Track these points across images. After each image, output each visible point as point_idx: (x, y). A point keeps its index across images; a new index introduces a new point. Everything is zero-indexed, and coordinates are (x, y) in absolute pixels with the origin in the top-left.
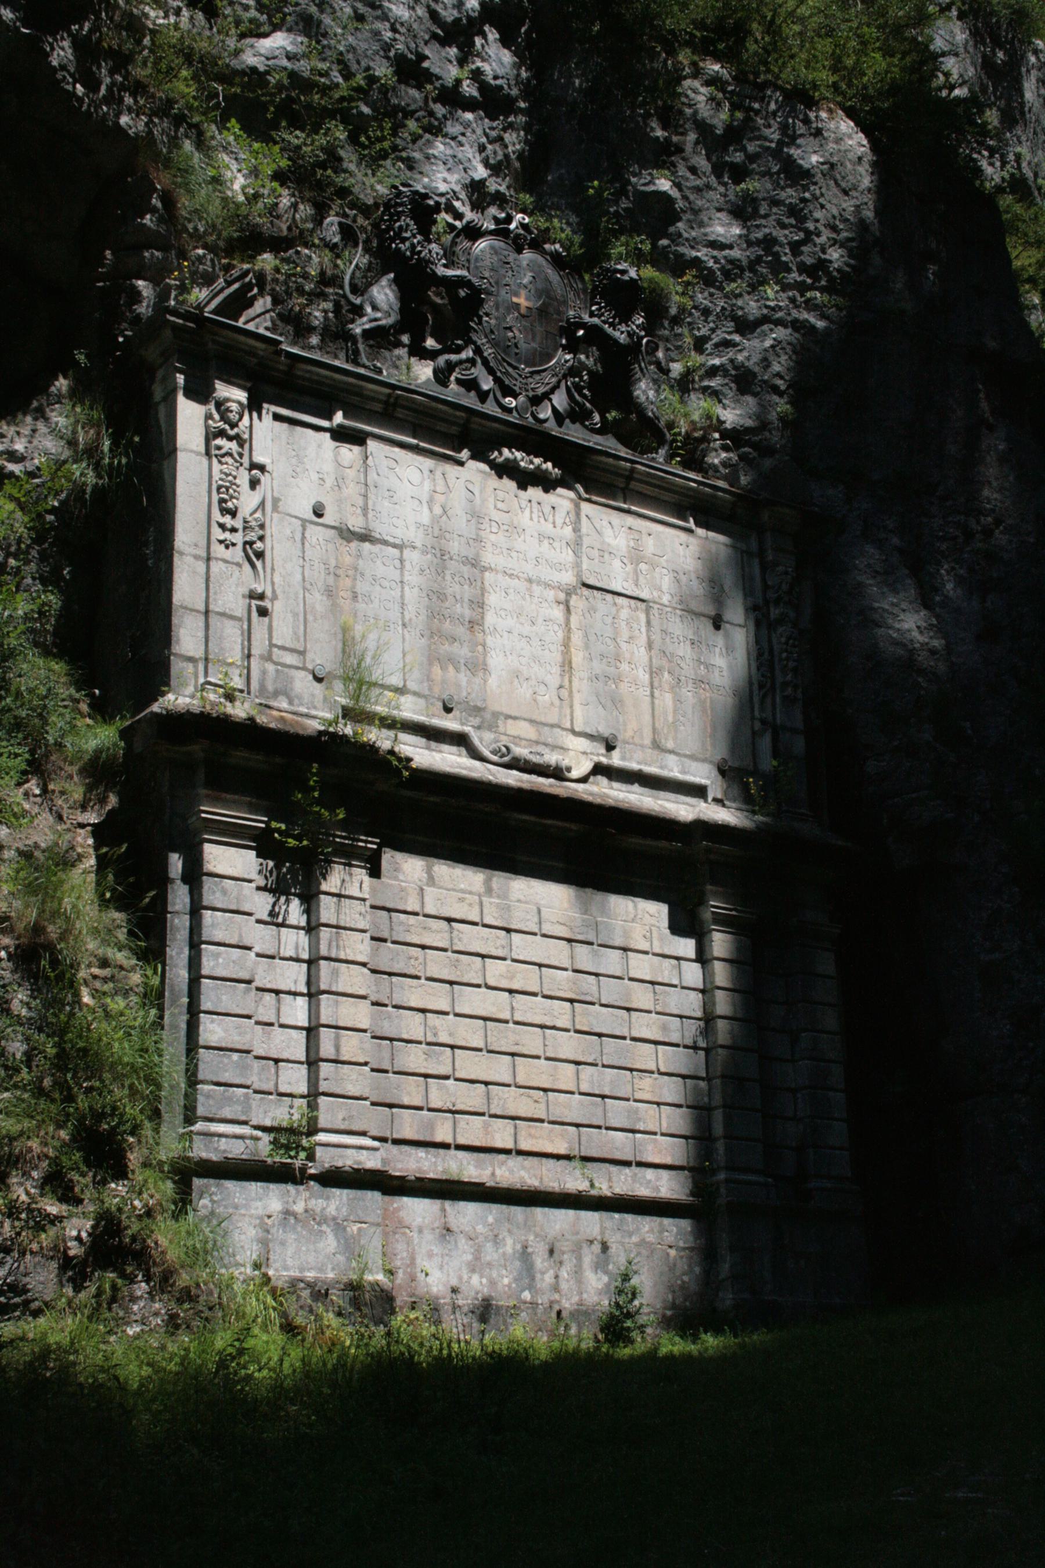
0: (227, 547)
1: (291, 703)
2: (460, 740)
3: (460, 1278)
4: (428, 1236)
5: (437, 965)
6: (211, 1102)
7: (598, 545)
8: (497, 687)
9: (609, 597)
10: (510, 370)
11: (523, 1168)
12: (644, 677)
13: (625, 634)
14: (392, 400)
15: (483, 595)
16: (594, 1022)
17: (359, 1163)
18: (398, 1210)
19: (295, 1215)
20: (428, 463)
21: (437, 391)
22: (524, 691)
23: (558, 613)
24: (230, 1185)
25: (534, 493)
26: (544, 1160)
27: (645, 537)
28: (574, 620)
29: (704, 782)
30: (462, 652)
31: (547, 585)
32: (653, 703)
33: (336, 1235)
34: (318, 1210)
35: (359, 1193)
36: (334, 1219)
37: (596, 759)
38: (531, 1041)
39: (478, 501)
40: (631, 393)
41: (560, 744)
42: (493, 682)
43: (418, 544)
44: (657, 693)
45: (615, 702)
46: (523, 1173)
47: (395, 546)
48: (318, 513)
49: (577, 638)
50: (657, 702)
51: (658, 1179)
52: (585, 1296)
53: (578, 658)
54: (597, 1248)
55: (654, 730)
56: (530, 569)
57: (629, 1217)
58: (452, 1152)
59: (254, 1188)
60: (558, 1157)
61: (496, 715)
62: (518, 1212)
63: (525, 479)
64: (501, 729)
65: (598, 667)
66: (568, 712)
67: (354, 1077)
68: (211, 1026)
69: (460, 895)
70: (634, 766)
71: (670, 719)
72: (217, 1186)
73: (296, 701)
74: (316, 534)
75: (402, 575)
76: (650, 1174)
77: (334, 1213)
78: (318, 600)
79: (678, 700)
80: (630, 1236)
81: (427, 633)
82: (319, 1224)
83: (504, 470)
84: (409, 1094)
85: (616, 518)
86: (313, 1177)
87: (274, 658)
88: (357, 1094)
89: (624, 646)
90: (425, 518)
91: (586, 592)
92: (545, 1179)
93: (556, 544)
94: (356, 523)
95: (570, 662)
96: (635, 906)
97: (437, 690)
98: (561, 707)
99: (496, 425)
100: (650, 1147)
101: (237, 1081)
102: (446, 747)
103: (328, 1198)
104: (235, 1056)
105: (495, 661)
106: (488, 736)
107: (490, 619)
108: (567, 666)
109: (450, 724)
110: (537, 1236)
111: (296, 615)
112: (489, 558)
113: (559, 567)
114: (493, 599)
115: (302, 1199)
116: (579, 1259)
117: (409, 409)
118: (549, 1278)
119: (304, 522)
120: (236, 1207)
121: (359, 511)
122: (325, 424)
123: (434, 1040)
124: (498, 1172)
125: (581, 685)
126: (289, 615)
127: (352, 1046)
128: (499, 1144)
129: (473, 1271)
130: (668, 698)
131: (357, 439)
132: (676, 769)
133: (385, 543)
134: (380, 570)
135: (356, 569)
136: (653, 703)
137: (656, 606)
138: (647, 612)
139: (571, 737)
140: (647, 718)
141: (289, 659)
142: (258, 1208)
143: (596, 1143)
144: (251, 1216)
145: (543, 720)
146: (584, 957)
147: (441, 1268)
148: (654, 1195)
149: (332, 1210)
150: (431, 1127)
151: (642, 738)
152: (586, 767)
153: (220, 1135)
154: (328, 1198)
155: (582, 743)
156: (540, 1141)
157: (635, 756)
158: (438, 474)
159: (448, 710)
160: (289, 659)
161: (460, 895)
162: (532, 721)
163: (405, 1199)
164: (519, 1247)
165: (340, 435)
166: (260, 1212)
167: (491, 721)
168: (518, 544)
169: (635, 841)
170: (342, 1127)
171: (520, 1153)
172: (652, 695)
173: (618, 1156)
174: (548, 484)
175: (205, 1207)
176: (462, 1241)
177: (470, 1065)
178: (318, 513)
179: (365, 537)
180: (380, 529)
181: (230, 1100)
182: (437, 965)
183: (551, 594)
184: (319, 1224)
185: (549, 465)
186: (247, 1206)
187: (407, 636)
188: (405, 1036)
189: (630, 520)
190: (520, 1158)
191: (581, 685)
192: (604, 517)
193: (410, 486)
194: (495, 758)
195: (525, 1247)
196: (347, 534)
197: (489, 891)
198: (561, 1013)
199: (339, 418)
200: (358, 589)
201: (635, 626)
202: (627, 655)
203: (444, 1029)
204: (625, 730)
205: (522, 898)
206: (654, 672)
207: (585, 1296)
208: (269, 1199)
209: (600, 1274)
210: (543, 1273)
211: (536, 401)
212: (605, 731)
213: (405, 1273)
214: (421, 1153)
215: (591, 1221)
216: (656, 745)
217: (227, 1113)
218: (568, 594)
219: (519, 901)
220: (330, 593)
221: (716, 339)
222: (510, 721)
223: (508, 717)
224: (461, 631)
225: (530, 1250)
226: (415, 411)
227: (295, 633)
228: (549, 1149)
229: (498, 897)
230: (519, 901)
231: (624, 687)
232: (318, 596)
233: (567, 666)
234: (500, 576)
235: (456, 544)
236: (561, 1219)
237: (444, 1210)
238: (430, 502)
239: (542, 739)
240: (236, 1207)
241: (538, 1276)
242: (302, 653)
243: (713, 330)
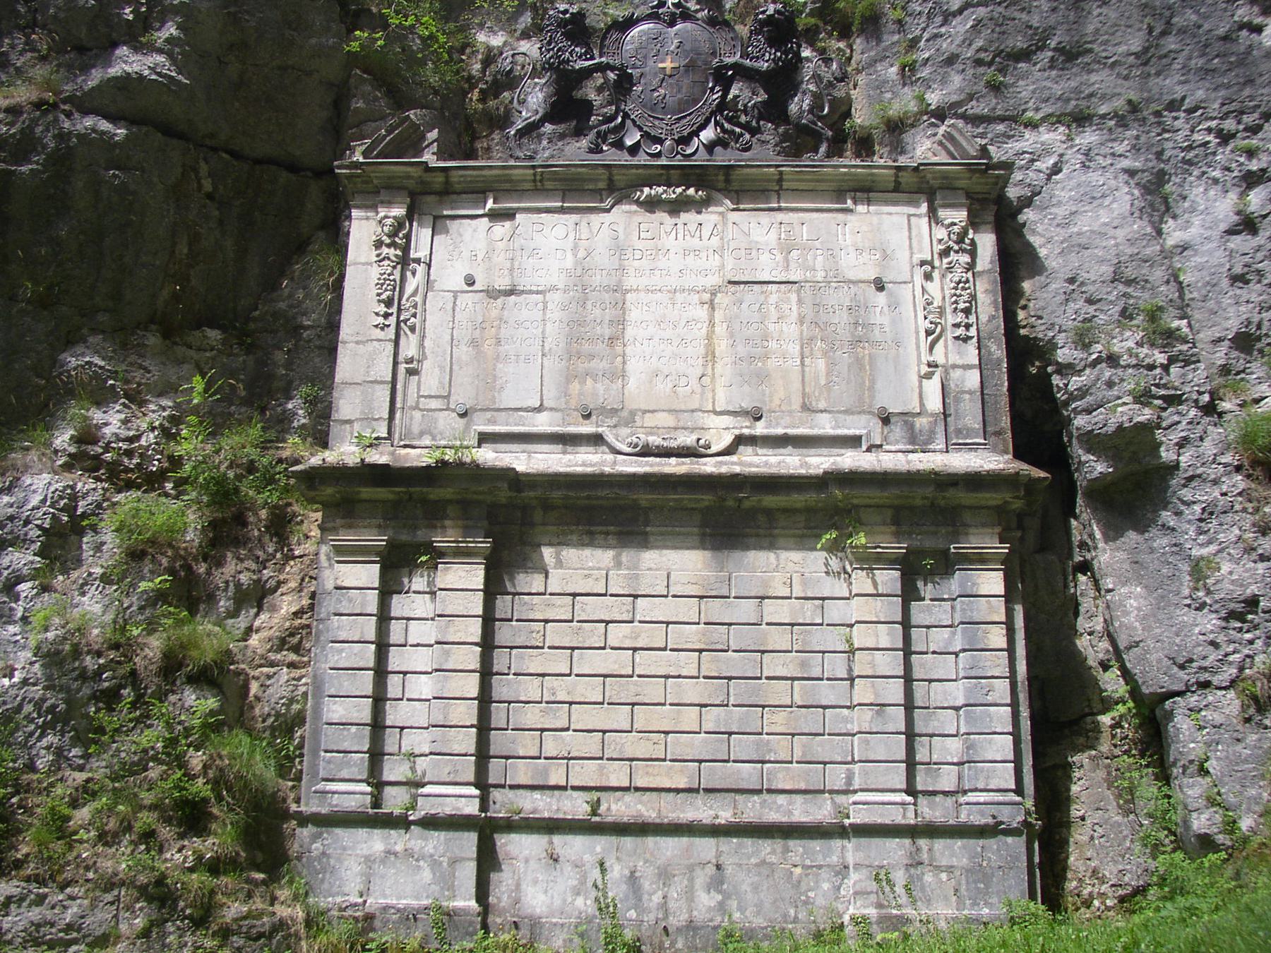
0: (382, 329)
1: (434, 439)
2: (596, 440)
3: (564, 901)
4: (533, 864)
5: (555, 635)
6: (332, 766)
7: (743, 246)
8: (636, 389)
9: (756, 287)
10: (657, 123)
11: (641, 802)
12: (795, 349)
13: (774, 314)
14: (538, 178)
15: (624, 313)
16: (724, 668)
17: (458, 809)
18: (505, 845)
19: (395, 854)
20: (574, 217)
21: (596, 159)
22: (663, 387)
23: (703, 313)
24: (338, 831)
25: (689, 217)
26: (663, 794)
27: (797, 227)
28: (718, 316)
29: (857, 432)
30: (599, 365)
31: (691, 290)
32: (803, 371)
33: (432, 869)
34: (417, 849)
35: (458, 834)
36: (431, 856)
37: (737, 432)
38: (653, 691)
39: (622, 237)
40: (787, 107)
41: (700, 425)
42: (632, 384)
43: (561, 286)
44: (807, 361)
45: (762, 377)
46: (639, 807)
47: (538, 292)
48: (470, 281)
49: (720, 329)
50: (807, 369)
51: (790, 804)
52: (695, 913)
53: (722, 346)
54: (711, 870)
55: (804, 394)
56: (674, 282)
57: (748, 842)
58: (569, 792)
59: (362, 833)
60: (678, 791)
61: (633, 413)
62: (628, 842)
63: (676, 207)
64: (639, 424)
65: (742, 350)
66: (710, 395)
67: (461, 737)
68: (334, 707)
69: (586, 572)
70: (780, 431)
71: (823, 382)
72: (328, 833)
73: (439, 437)
74: (466, 300)
75: (544, 314)
76: (781, 799)
77: (432, 851)
78: (463, 352)
79: (831, 364)
80: (749, 859)
81: (565, 357)
82: (417, 860)
83: (651, 205)
84: (524, 746)
85: (765, 218)
86: (415, 823)
87: (421, 406)
88: (463, 752)
89: (771, 327)
90: (569, 262)
91: (732, 288)
92: (664, 812)
93: (703, 255)
94: (502, 283)
95: (713, 353)
96: (778, 558)
97: (573, 404)
98: (703, 394)
99: (640, 171)
100: (780, 775)
101: (355, 749)
102: (583, 449)
103: (426, 839)
104: (354, 729)
105: (634, 366)
106: (624, 431)
107: (630, 332)
108: (710, 355)
109: (587, 428)
110: (646, 861)
111: (441, 368)
112: (630, 281)
113: (705, 273)
114: (634, 315)
115: (398, 840)
116: (691, 880)
117: (555, 180)
118: (657, 898)
119: (455, 294)
120: (344, 849)
121: (506, 272)
122: (480, 212)
123: (553, 699)
124: (613, 807)
125: (724, 369)
126: (437, 370)
127: (947, 722)
128: (615, 783)
129: (578, 894)
130: (821, 364)
131: (509, 215)
132: (828, 426)
133: (531, 292)
134: (525, 314)
135: (501, 319)
136: (803, 371)
137: (808, 285)
138: (798, 292)
139: (713, 416)
140: (797, 385)
141: (434, 404)
142: (363, 849)
143: (715, 775)
144: (357, 855)
145: (683, 408)
146: (715, 610)
147: (546, 892)
148: (785, 819)
149: (429, 848)
150: (546, 772)
151: (790, 404)
152: (727, 439)
153: (334, 793)
154: (426, 839)
155: (727, 420)
156: (658, 778)
157: (782, 422)
158: (584, 224)
159: (587, 416)
160: (434, 404)
161: (586, 572)
162: (670, 411)
163: (513, 835)
164: (627, 872)
165: (495, 216)
166: (365, 852)
167: (623, 415)
168: (662, 263)
169: (770, 501)
170: (448, 780)
171: (637, 789)
172: (802, 364)
173: (744, 785)
174: (700, 206)
175: (317, 849)
176: (568, 868)
177: (583, 716)
178: (470, 281)
179: (511, 292)
180: (524, 283)
181: (348, 764)
182: (555, 635)
183: (695, 298)
184: (417, 860)
185: (691, 191)
186: (353, 848)
187: (546, 363)
188: (522, 699)
189: (780, 216)
190: (638, 794)
191: (724, 369)
192: (752, 220)
193: (550, 242)
194: (629, 450)
195: (633, 873)
196: (492, 294)
197: (618, 565)
198: (688, 663)
199: (490, 204)
200: (501, 336)
201: (785, 306)
202: (776, 335)
203: (562, 688)
204: (771, 401)
205: (653, 566)
206: (806, 343)
207: (695, 913)
208: (375, 842)
209: (713, 893)
210: (650, 895)
211: (685, 141)
212: (747, 405)
213: (509, 897)
214: (537, 795)
215: (706, 847)
216: (806, 408)
217: (345, 774)
218: (713, 294)
219: (650, 569)
220: (474, 343)
221: (926, 36)
222: (648, 415)
223: (645, 412)
224: (601, 347)
225: (637, 874)
226: (560, 180)
227: (440, 382)
228: (667, 784)
229: (628, 569)
230: (650, 569)
231: (772, 363)
232: (465, 349)
233: (710, 355)
234: (642, 294)
235: (599, 277)
236: (669, 846)
237: (551, 843)
238: (575, 249)
239: (681, 424)
240: (344, 849)
241: (646, 897)
242: (447, 397)
243: (924, 30)
